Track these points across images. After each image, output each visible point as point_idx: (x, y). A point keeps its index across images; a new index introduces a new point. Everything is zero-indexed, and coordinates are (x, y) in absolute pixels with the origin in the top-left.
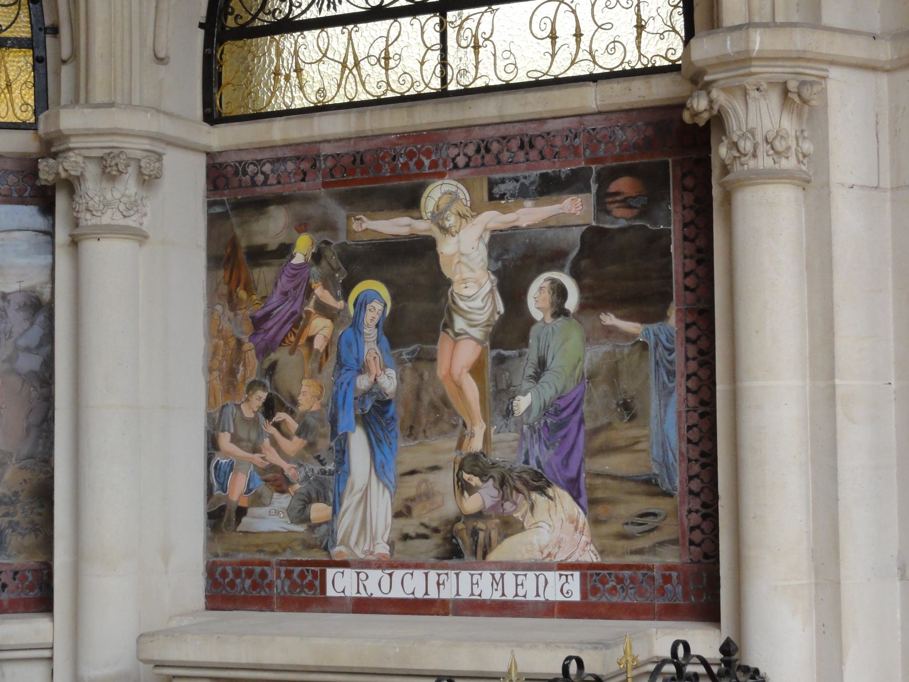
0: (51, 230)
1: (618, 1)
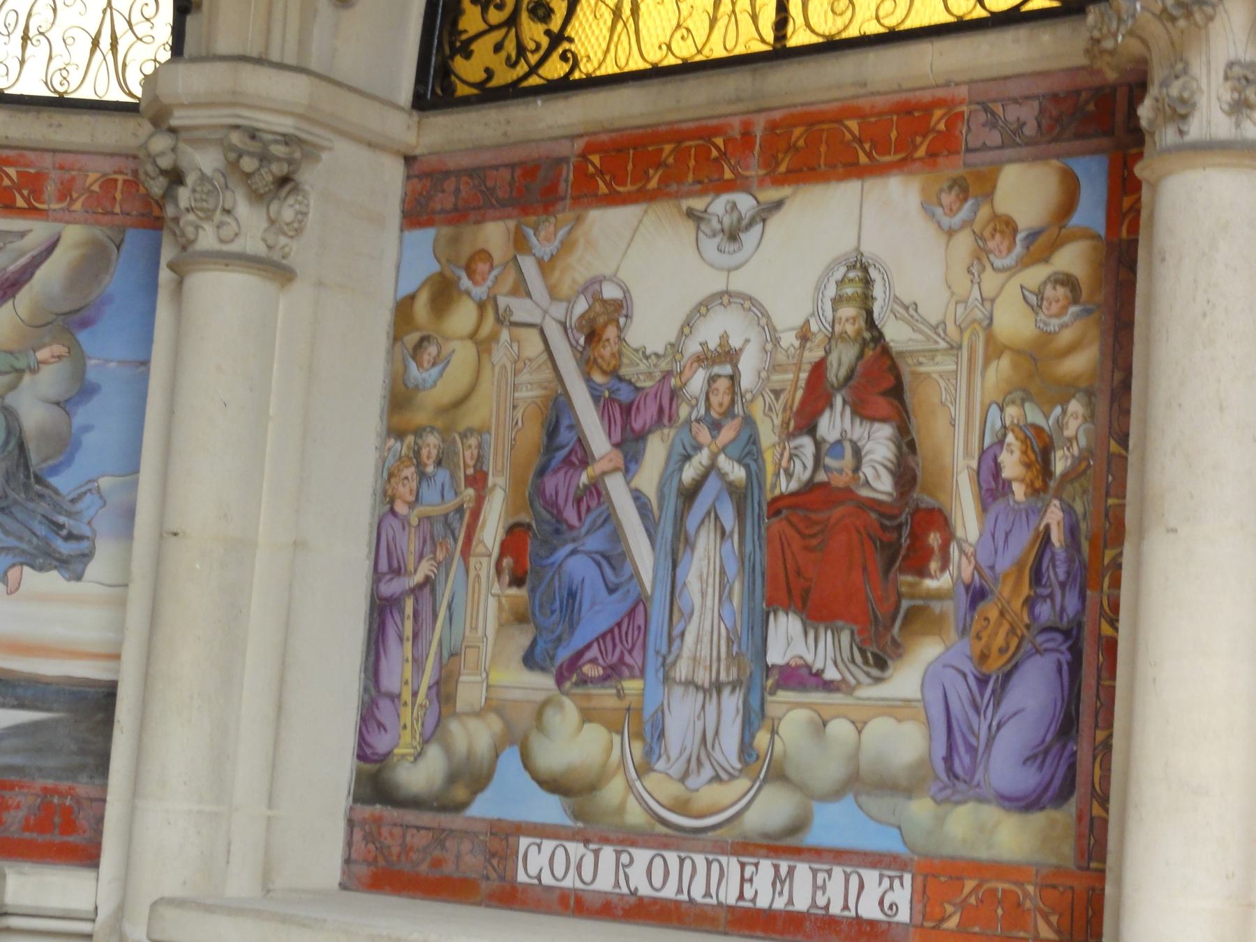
0: (511, 264)
1: (1, 62)
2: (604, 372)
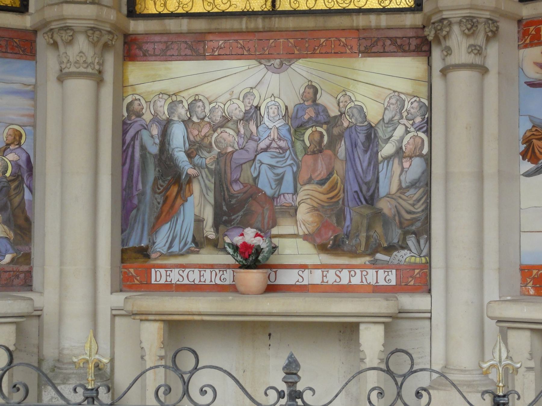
2: (198, 118)
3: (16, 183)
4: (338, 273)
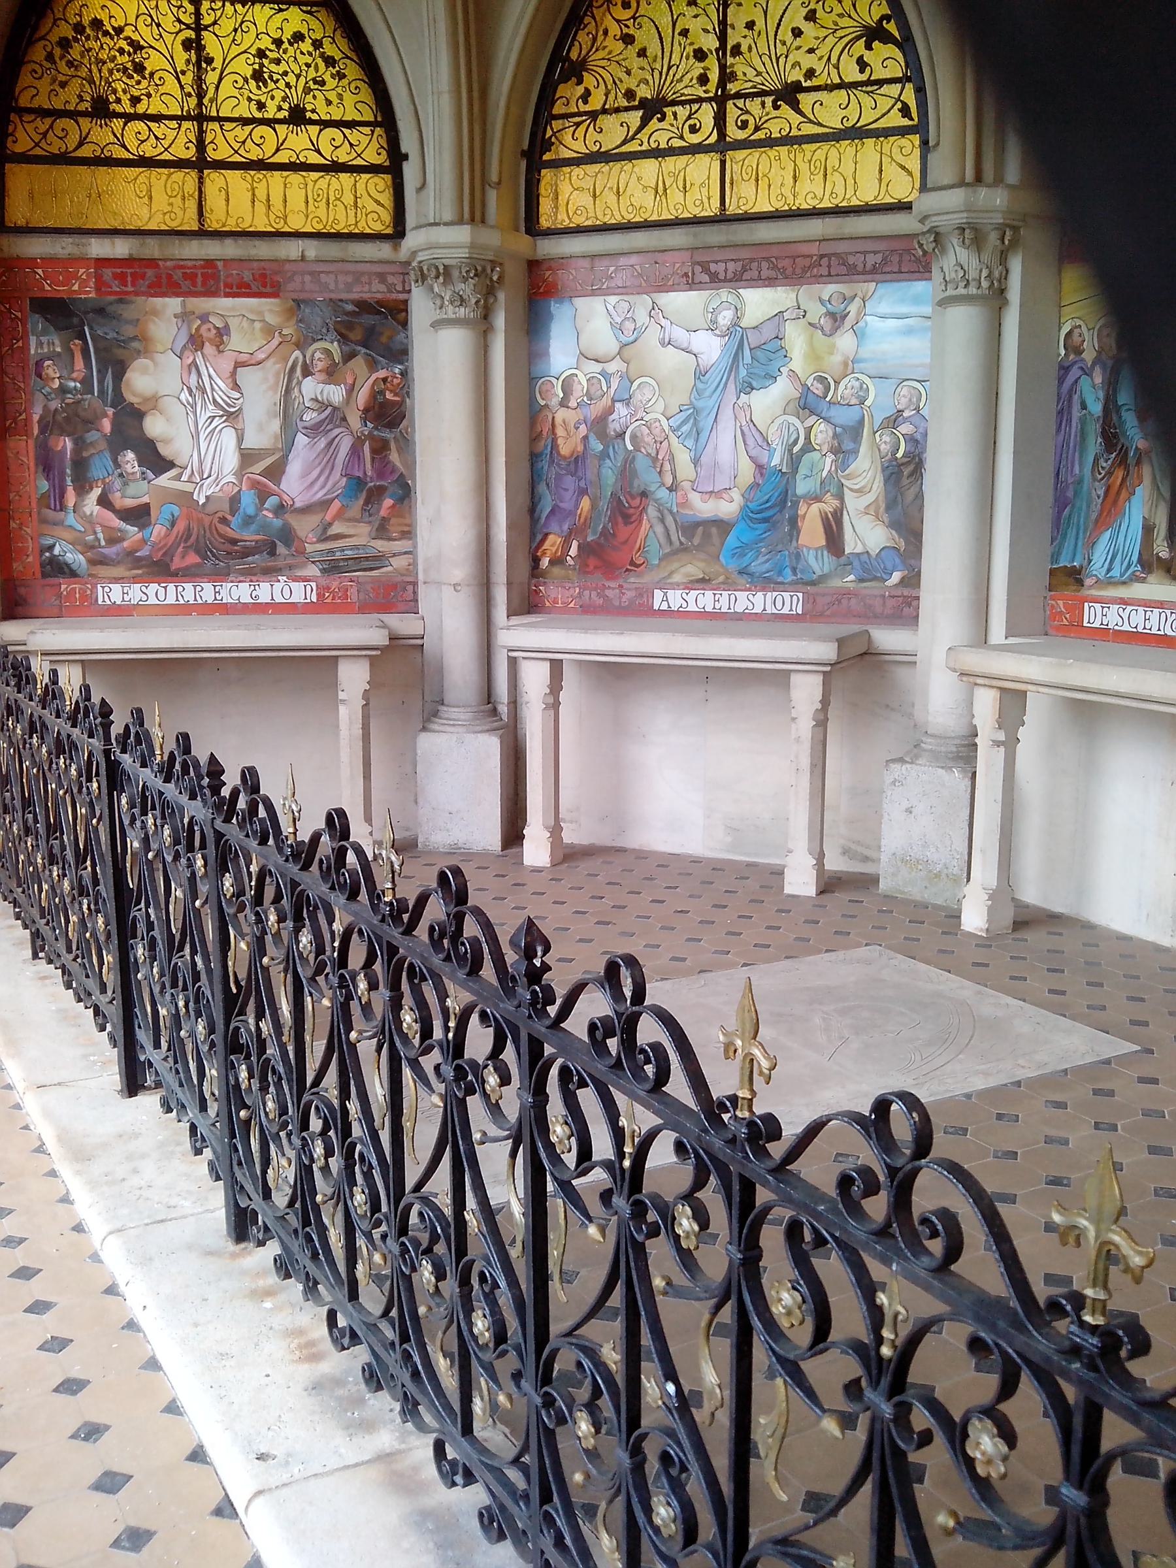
3: (911, 467)
4: (144, 589)
